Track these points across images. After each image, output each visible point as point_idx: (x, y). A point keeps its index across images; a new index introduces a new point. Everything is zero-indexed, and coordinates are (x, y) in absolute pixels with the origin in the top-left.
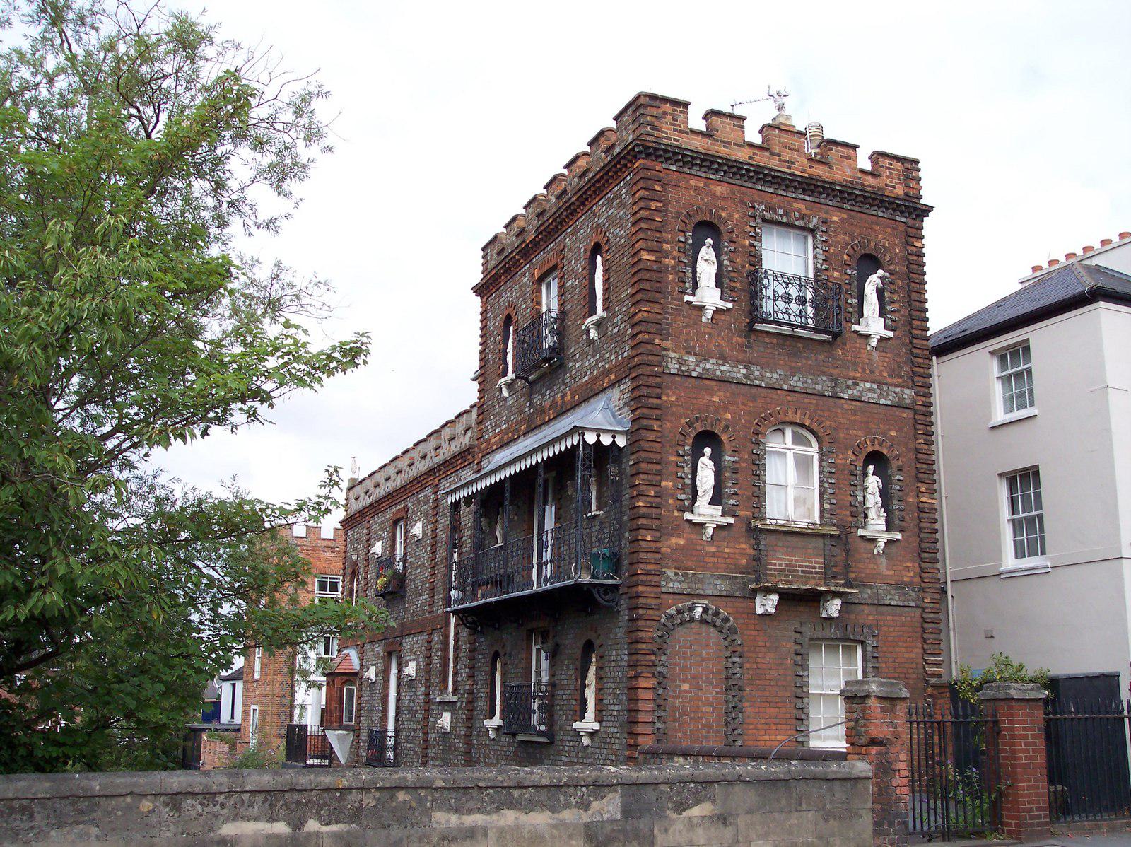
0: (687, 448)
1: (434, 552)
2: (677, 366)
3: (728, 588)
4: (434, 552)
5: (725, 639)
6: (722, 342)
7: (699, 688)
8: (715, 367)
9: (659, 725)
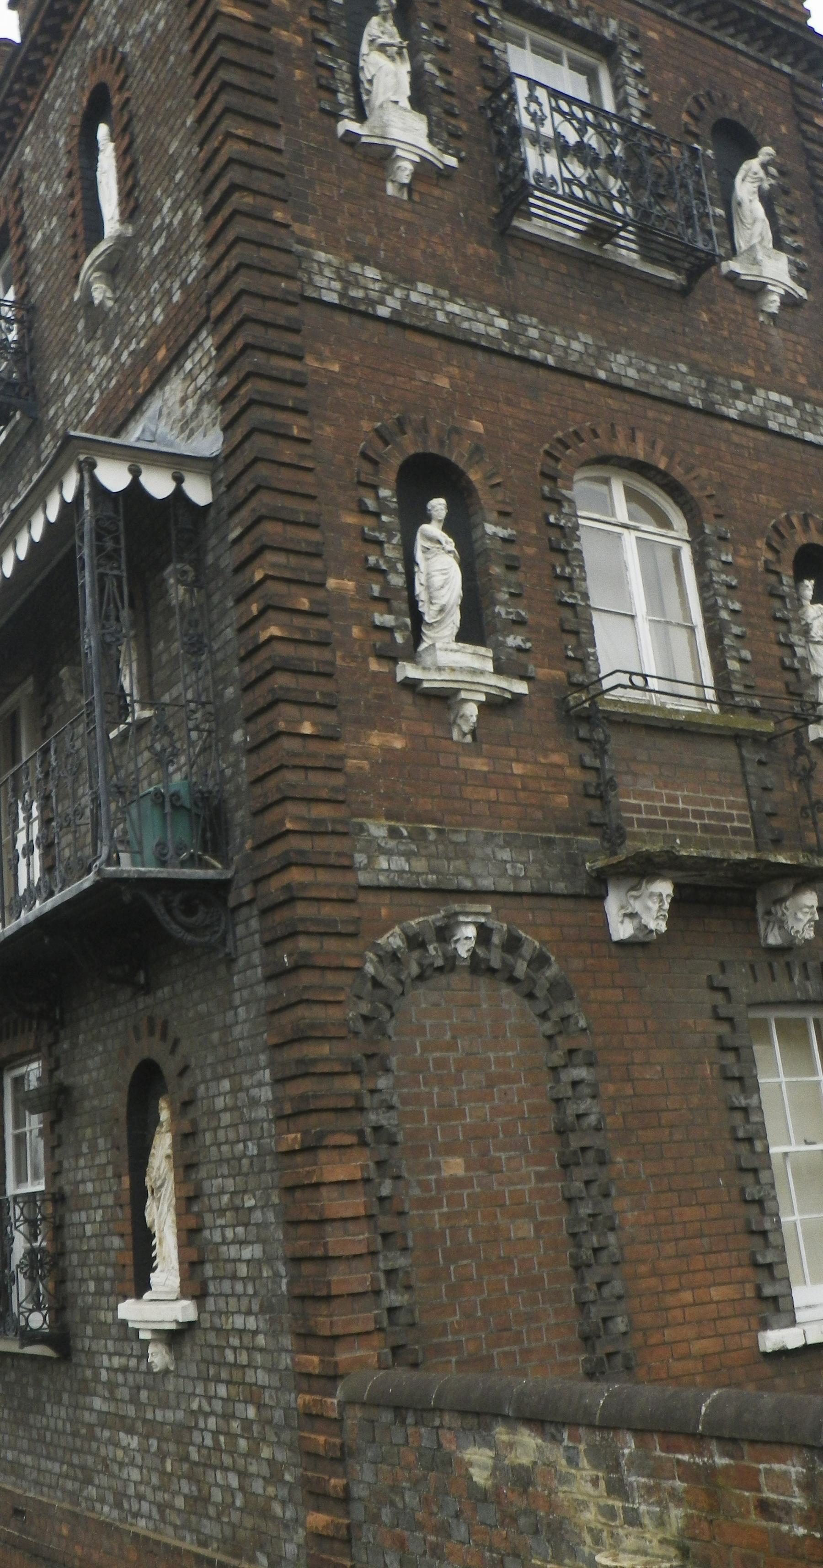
0: (384, 493)
2: (336, 285)
5: (544, 1016)
6: (441, 250)
7: (490, 1166)
8: (433, 303)
9: (393, 1298)
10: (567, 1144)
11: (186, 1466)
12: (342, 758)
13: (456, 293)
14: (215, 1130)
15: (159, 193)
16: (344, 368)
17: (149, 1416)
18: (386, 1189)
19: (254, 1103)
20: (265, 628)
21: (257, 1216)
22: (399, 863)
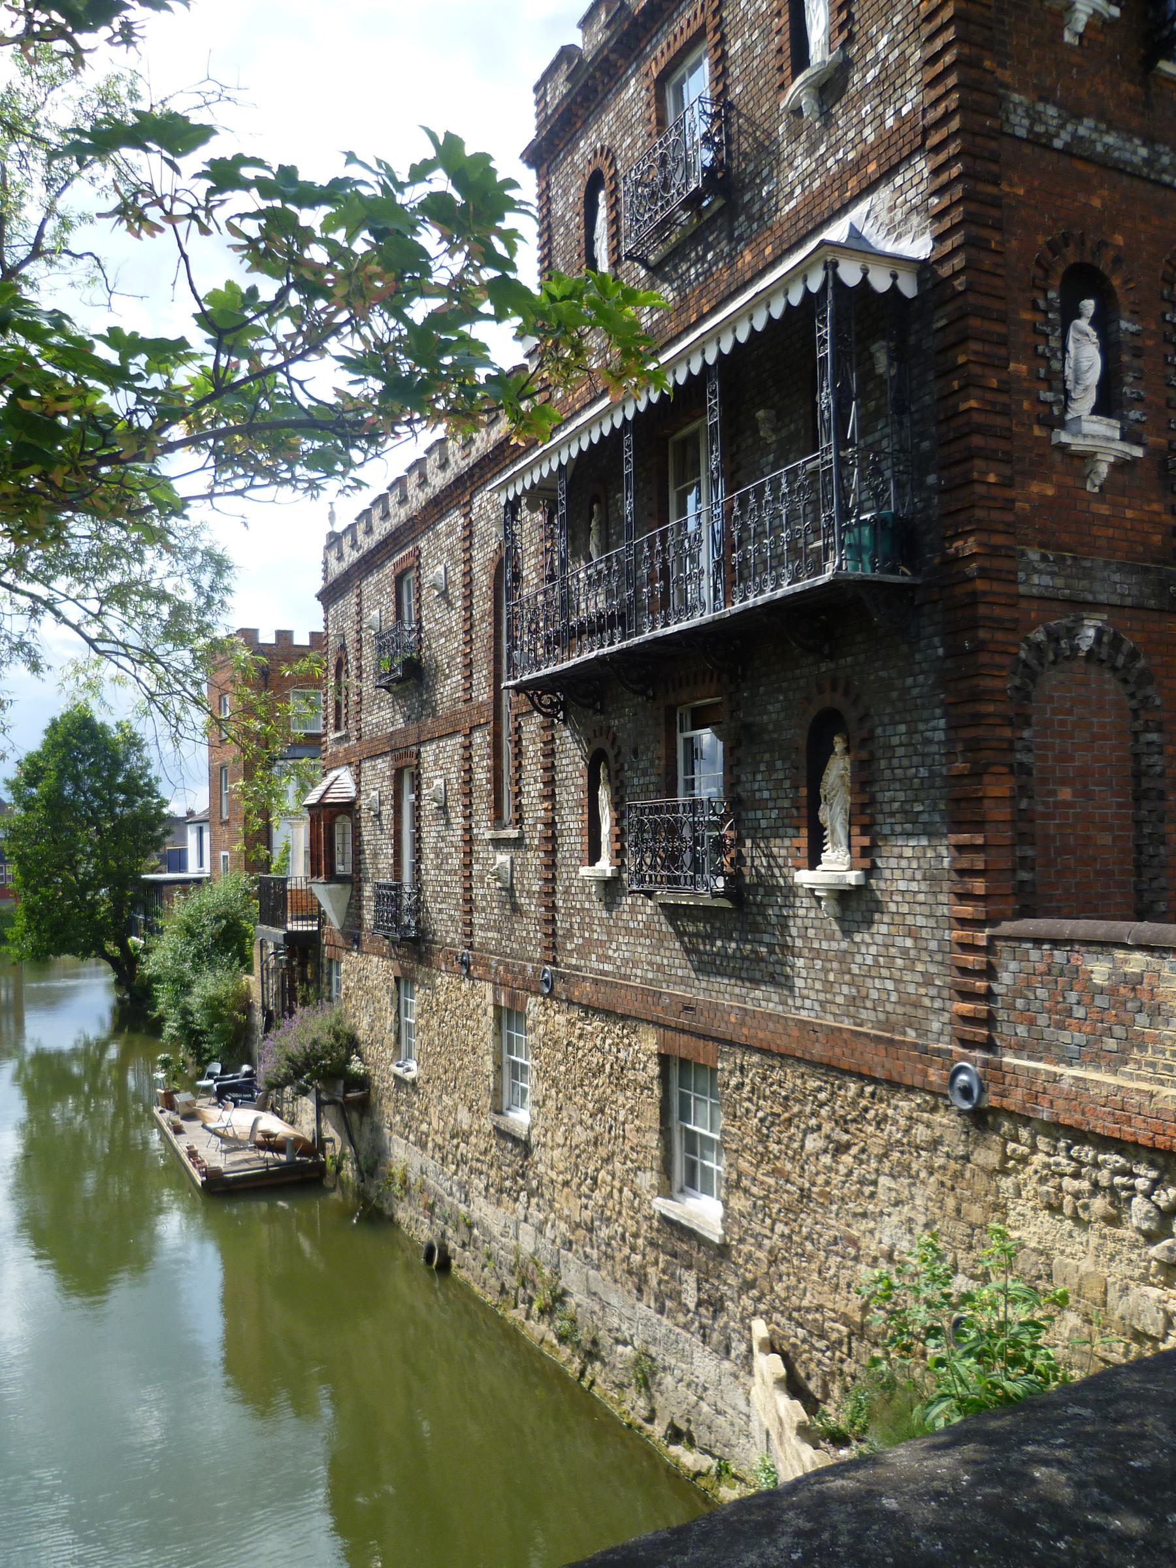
0: (1052, 295)
1: (468, 608)
2: (1026, 122)
3: (1135, 591)
4: (468, 608)
5: (1132, 696)
6: (1101, 88)
8: (1094, 136)
9: (1024, 875)
10: (1139, 785)
11: (847, 977)
12: (1013, 501)
13: (1111, 127)
14: (890, 759)
15: (874, 29)
16: (1028, 192)
17: (816, 945)
18: (1024, 804)
19: (928, 741)
20: (966, 400)
21: (924, 818)
22: (1046, 580)
